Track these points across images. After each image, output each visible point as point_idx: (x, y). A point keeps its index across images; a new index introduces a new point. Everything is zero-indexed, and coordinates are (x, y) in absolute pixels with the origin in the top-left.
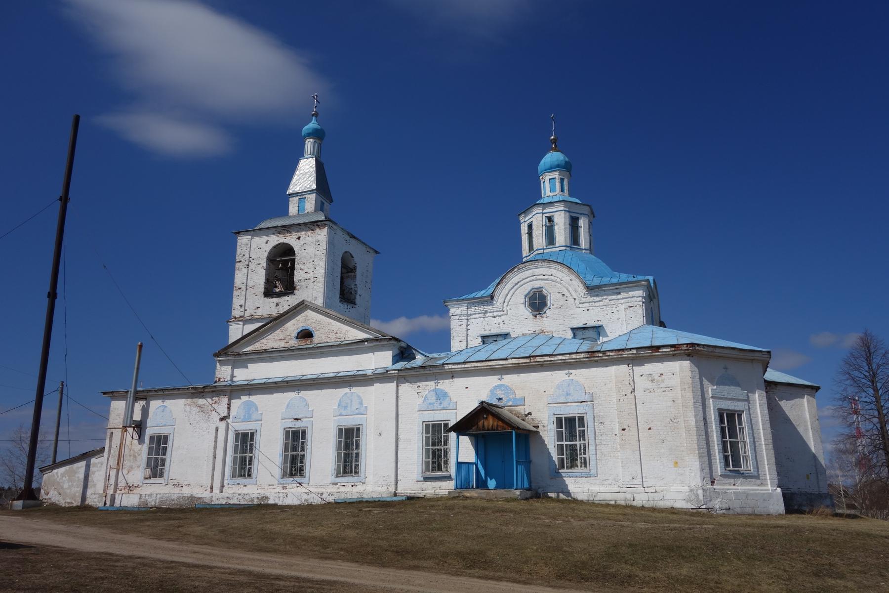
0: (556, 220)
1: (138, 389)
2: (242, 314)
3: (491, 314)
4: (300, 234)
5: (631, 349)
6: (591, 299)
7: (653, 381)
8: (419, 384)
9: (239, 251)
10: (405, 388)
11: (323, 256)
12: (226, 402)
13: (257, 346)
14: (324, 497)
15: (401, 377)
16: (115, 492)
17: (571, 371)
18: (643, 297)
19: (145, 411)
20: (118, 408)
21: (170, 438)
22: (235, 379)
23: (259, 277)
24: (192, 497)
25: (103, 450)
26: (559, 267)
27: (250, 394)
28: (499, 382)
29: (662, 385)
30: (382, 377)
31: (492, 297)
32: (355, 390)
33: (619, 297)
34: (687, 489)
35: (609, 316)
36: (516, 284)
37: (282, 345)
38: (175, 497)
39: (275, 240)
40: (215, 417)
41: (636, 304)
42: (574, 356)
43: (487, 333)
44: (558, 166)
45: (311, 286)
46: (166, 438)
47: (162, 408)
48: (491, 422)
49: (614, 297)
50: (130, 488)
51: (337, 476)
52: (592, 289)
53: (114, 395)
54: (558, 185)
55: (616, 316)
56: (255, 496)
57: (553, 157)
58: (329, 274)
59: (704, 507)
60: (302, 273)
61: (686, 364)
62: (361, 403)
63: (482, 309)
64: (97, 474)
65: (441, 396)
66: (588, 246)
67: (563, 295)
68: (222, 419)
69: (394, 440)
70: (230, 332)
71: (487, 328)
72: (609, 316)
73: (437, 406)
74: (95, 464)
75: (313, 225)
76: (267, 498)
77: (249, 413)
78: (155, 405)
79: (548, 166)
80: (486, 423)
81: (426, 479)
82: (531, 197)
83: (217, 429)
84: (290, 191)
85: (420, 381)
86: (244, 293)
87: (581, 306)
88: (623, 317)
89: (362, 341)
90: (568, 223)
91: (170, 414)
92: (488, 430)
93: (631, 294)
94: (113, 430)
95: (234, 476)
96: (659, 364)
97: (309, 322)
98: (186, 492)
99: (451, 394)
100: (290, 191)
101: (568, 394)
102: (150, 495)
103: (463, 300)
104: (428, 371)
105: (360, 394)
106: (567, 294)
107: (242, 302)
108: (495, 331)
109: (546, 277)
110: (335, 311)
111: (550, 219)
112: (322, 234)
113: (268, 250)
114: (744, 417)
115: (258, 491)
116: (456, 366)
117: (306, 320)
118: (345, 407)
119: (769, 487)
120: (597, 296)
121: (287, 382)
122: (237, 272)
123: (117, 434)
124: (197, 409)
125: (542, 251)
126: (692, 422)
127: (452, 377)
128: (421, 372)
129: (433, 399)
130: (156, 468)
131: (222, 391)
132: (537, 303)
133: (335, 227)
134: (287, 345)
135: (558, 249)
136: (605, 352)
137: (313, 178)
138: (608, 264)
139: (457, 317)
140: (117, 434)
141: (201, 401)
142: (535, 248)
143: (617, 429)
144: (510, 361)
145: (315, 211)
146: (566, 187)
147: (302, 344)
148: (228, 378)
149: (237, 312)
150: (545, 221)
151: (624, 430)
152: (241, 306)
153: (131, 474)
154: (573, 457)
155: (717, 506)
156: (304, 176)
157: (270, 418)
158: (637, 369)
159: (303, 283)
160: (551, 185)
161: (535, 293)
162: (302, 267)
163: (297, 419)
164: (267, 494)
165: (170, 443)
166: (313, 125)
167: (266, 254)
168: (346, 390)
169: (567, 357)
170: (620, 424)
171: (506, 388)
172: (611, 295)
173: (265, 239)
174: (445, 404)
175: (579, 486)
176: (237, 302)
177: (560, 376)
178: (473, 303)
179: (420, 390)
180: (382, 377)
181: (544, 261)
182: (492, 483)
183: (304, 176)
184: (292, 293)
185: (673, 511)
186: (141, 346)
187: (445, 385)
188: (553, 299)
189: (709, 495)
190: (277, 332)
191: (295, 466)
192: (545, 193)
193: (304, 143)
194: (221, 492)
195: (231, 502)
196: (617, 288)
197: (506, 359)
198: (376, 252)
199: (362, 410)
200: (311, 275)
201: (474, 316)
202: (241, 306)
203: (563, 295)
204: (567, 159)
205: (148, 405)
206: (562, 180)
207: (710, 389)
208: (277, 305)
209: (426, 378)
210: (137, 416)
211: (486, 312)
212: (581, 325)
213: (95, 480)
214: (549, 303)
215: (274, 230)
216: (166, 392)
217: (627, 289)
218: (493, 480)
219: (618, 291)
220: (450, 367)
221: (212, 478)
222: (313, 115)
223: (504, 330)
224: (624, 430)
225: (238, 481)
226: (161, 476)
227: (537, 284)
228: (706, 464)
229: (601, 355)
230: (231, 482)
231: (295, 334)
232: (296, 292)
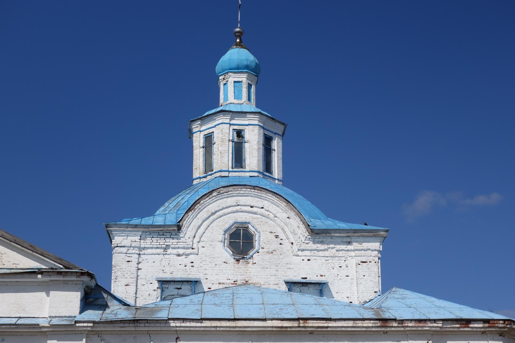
3: (175, 251)
5: (435, 321)
6: (315, 246)
18: (379, 251)
26: (274, 199)
33: (350, 247)
35: (335, 271)
36: (213, 214)
41: (371, 259)
42: (360, 324)
43: (167, 276)
44: (247, 67)
49: (343, 247)
52: (317, 234)
54: (245, 91)
55: (344, 272)
57: (237, 55)
66: (281, 177)
67: (277, 237)
71: (168, 269)
72: (335, 271)
79: (234, 64)
82: (205, 101)
87: (300, 253)
89: (33, 273)
93: (365, 245)
103: (136, 226)
104: (142, 328)
106: (282, 235)
108: (179, 275)
109: (254, 209)
110: (371, 225)
111: (239, 134)
116: (188, 324)
120: (322, 243)
125: (226, 174)
128: (131, 328)
132: (241, 241)
135: (248, 174)
136: (402, 321)
138: (313, 203)
139: (124, 250)
144: (269, 323)
146: (253, 97)
150: (232, 135)
160: (234, 90)
169: (350, 324)
172: (339, 244)
181: (254, 187)
188: (262, 239)
192: (226, 98)
196: (349, 237)
197: (264, 320)
203: (277, 237)
204: (257, 61)
206: (250, 86)
211: (167, 247)
212: (298, 279)
214: (256, 244)
219: (349, 240)
223: (192, 275)
227: (242, 217)
229: (395, 324)
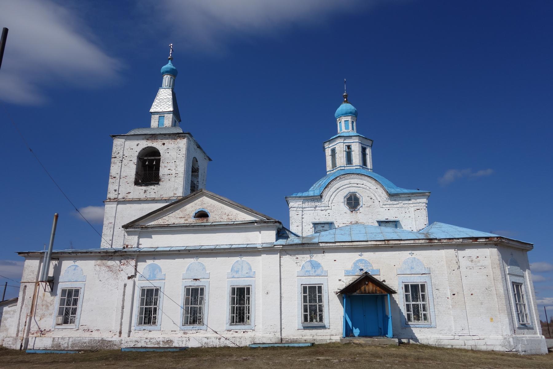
0: (353, 148)
1: (53, 251)
2: (116, 196)
3: (320, 208)
4: (164, 141)
5: (458, 239)
6: (391, 202)
7: (472, 261)
8: (297, 256)
9: (114, 149)
10: (287, 259)
11: (184, 159)
13: (160, 222)
15: (285, 251)
16: (28, 335)
17: (413, 252)
19: (58, 270)
20: (32, 267)
21: (81, 292)
22: (140, 246)
23: (130, 170)
24: (103, 340)
25: (16, 300)
26: (369, 179)
27: (154, 259)
28: (360, 258)
29: (478, 264)
30: (269, 250)
31: (321, 197)
32: (245, 259)
33: (410, 202)
34: (500, 337)
37: (182, 221)
38: (87, 340)
39: (144, 144)
40: (123, 276)
41: (422, 207)
42: (417, 241)
43: (317, 221)
44: (351, 113)
45: (173, 179)
46: (77, 292)
47: (73, 267)
48: (370, 287)
49: (407, 202)
50: (42, 332)
51: (231, 325)
53: (28, 255)
54: (350, 125)
56: (161, 339)
57: (345, 107)
58: (186, 172)
59: (514, 350)
60: (166, 169)
61: (495, 251)
62: (250, 269)
63: (313, 204)
64: (9, 320)
65: (316, 266)
66: (372, 168)
67: (371, 198)
68: (129, 278)
69: (279, 298)
71: (317, 217)
72: (403, 215)
73: (312, 273)
74: (7, 312)
75: (175, 136)
76: (171, 341)
77: (154, 272)
78: (66, 264)
79: (344, 112)
80: (367, 288)
81: (305, 328)
82: (331, 132)
83: (125, 285)
84: (152, 110)
85: (298, 254)
86: (118, 181)
87: (384, 206)
88: (413, 216)
90: (361, 151)
91: (75, 272)
92: (369, 293)
93: (418, 201)
94: (27, 284)
95: (140, 323)
96: (476, 250)
97: (205, 206)
98: (97, 336)
99: (322, 264)
100: (152, 110)
101: (412, 268)
102: (63, 338)
103: (300, 197)
104: (306, 247)
105: (250, 263)
106: (374, 198)
107: (117, 188)
108: (323, 220)
109: (359, 185)
111: (349, 147)
112: (183, 143)
113: (139, 151)
114: (523, 286)
115: (163, 336)
116: (329, 245)
117: (203, 203)
118: (237, 272)
119: (539, 335)
120: (395, 200)
121: (189, 250)
122: (112, 165)
123: (31, 288)
124: (107, 269)
125: (343, 168)
126: (502, 291)
127: (324, 252)
129: (309, 268)
130: (67, 314)
131: (130, 255)
132: (353, 202)
133: (191, 139)
134: (187, 222)
135: (355, 168)
136: (440, 240)
137: (171, 103)
139: (295, 209)
140: (31, 288)
141: (110, 263)
142: (338, 165)
143: (449, 294)
144: (369, 243)
145: (172, 126)
146: (355, 128)
147: (199, 221)
148: (136, 245)
149: (111, 195)
150: (345, 148)
151: (454, 295)
152: (115, 191)
153: (43, 320)
154: (418, 313)
155: (520, 350)
156: (163, 101)
157: (172, 280)
158: (461, 253)
159: (167, 177)
160: (345, 125)
161: (351, 196)
162: (166, 165)
163: (196, 280)
164: (172, 338)
165: (324, 292)
166: (169, 65)
167: (137, 154)
168: (238, 259)
169: (412, 242)
170: (451, 290)
171: (366, 262)
173: (136, 142)
174: (319, 272)
175: (423, 334)
176: (112, 187)
177: (405, 255)
178: (307, 200)
179: (298, 261)
180: (269, 250)
181: (358, 174)
182: (356, 332)
183: (163, 101)
184: (158, 184)
185: (492, 352)
186: (57, 216)
187: (318, 258)
188: (364, 200)
189: (517, 340)
190: (178, 211)
191: (193, 316)
192: (341, 130)
193: (162, 78)
194: (129, 336)
195: (139, 345)
196: (409, 197)
197: (367, 241)
198: (210, 160)
200: (173, 172)
201: (307, 209)
202: (115, 191)
203: (371, 198)
205: (60, 264)
206: (353, 122)
207: (507, 268)
208: (145, 191)
209: (303, 252)
210: (51, 274)
211: (316, 206)
212: (384, 219)
213: (7, 325)
214: (361, 203)
215: (144, 137)
216: (79, 255)
217: (416, 197)
218: (358, 329)
219: (409, 198)
220: (324, 245)
221: (121, 325)
222: (169, 59)
223: (329, 220)
224: (454, 295)
226: (72, 322)
227: (353, 190)
228: (511, 321)
229: (436, 241)
230: (138, 328)
231: (193, 214)
232: (160, 183)
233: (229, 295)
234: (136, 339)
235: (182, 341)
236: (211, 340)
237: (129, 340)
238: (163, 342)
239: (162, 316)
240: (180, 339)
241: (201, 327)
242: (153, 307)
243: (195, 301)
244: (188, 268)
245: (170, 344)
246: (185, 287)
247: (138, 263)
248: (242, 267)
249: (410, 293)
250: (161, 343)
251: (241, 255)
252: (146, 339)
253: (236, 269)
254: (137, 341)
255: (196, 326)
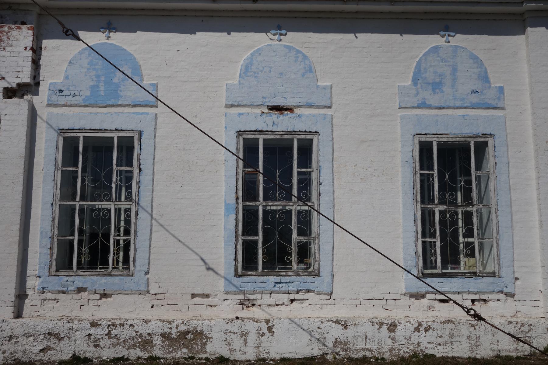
12: (29, 42)
14: (400, 332)
27: (110, 27)
56: (156, 327)
62: (485, 78)
70: (29, 261)
76: (200, 336)
95: (64, 263)
104: (262, 133)
105: (481, 56)
118: (436, 86)
194: (18, 315)
199: (490, 96)
225: (79, 282)
230: (55, 283)
233: (409, 170)
234: (50, 326)
235: (244, 335)
236: (360, 331)
237: (18, 331)
238: (165, 336)
239: (152, 242)
240: (234, 327)
241: (310, 282)
242: (295, 207)
243: (279, 187)
244: (247, 69)
245: (197, 347)
246: (239, 133)
247: (45, 43)
248: (455, 70)
249: (435, 172)
250: (158, 341)
251: (447, 29)
252: (94, 325)
253: (430, 76)
254: (57, 336)
255: (293, 280)
